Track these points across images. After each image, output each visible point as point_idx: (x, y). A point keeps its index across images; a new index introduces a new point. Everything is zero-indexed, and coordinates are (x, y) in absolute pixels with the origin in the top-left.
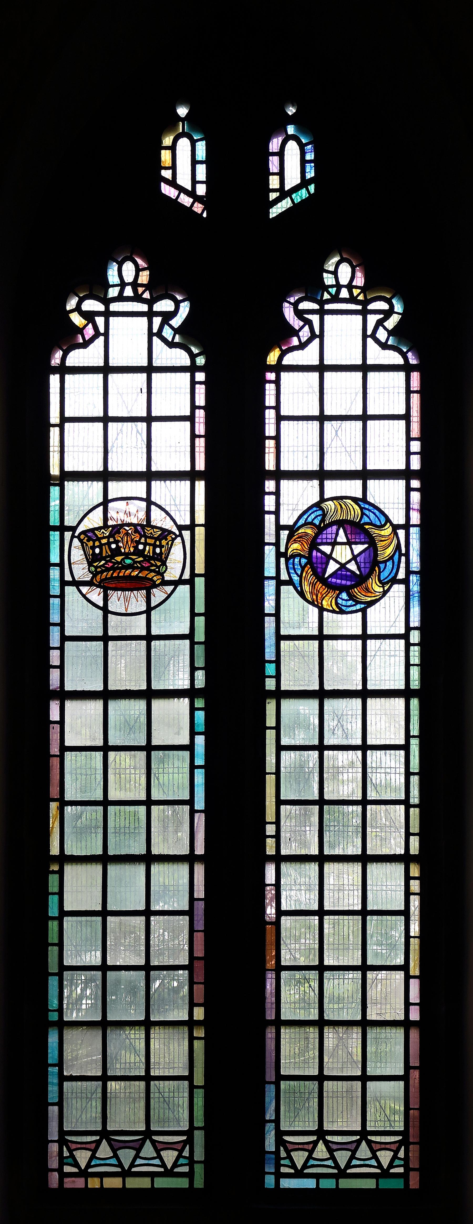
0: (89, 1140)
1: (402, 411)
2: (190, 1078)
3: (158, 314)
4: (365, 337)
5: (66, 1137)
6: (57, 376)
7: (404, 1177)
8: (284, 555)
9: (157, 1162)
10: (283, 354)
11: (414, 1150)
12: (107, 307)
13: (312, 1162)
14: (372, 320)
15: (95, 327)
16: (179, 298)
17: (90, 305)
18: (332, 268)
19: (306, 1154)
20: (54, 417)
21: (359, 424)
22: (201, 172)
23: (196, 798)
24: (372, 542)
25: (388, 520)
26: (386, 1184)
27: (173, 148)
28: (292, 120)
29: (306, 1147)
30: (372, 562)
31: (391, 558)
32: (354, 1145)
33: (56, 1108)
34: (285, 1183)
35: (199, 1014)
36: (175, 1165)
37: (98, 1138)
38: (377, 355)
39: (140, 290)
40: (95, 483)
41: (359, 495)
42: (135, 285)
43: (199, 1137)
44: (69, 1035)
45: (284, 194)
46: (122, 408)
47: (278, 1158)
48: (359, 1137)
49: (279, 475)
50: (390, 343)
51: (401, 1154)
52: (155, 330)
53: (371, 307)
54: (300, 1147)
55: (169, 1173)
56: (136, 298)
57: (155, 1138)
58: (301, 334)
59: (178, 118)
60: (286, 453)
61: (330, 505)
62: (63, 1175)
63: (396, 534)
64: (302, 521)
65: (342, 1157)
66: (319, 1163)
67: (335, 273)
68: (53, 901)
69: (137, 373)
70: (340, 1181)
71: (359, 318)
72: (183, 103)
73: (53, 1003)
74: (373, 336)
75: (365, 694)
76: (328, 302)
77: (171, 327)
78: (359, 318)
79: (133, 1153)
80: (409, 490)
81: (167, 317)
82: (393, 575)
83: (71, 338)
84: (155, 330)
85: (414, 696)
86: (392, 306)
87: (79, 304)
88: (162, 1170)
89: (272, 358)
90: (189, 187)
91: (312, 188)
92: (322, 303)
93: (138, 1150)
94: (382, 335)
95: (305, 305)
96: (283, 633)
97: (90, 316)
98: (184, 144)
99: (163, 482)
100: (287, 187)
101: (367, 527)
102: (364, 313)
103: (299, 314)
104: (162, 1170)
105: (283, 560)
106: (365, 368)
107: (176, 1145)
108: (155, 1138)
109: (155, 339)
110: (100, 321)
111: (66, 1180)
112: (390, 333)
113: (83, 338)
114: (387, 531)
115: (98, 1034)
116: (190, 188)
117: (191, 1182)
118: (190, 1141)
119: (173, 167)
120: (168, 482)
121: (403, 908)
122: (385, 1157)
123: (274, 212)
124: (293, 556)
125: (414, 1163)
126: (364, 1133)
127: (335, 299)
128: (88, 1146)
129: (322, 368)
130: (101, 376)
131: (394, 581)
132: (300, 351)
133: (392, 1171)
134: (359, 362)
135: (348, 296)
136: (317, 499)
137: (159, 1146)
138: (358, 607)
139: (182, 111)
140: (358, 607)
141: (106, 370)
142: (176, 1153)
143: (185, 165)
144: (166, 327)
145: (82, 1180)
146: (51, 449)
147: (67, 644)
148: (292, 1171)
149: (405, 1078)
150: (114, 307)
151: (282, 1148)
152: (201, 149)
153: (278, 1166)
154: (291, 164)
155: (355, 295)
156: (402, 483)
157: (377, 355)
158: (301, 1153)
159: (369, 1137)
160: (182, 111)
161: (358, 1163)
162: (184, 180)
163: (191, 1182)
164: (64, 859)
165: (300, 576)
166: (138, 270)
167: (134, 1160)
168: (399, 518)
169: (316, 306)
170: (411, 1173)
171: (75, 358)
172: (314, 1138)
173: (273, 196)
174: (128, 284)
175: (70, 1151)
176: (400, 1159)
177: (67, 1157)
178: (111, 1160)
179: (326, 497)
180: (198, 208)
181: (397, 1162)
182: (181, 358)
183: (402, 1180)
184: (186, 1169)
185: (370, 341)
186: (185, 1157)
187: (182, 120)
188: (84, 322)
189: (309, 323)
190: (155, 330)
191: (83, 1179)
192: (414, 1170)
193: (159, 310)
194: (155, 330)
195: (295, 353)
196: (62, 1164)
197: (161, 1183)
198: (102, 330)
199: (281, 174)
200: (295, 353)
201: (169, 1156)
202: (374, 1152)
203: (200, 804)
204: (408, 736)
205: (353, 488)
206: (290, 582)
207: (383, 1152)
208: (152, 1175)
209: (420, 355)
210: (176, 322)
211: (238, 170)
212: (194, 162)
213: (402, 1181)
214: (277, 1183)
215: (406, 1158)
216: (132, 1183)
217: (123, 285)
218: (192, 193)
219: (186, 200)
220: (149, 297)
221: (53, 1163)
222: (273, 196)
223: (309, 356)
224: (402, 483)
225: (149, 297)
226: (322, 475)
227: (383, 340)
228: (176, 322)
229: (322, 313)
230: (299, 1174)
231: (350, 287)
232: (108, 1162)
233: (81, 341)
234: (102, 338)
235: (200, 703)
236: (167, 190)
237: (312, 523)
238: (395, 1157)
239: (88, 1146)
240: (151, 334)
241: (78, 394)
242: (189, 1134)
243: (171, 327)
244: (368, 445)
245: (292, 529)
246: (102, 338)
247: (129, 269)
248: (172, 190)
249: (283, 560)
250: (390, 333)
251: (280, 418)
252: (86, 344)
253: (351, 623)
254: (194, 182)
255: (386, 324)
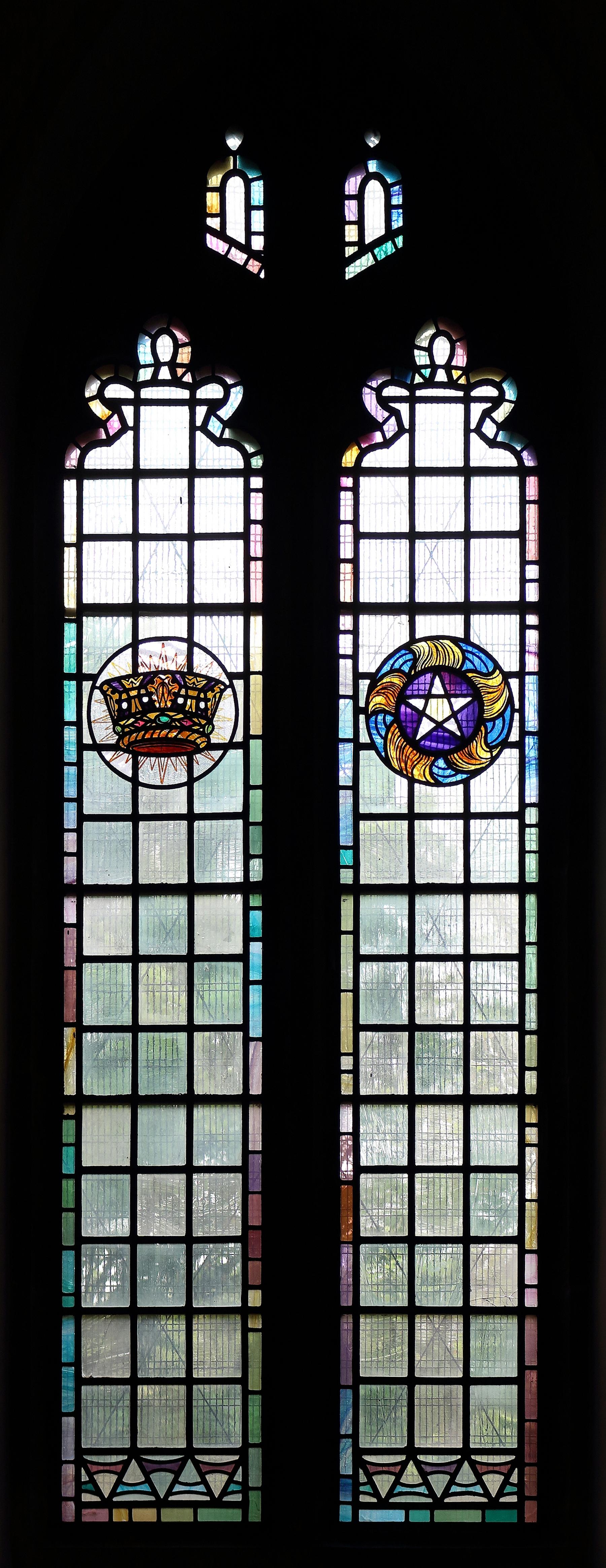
0: (113, 1461)
1: (516, 527)
2: (243, 1381)
3: (203, 402)
4: (467, 431)
5: (85, 1457)
6: (73, 482)
7: (518, 1507)
8: (364, 710)
9: (201, 1488)
10: (363, 453)
11: (531, 1473)
12: (137, 394)
13: (399, 1489)
14: (477, 409)
15: (122, 419)
16: (230, 381)
17: (115, 391)
18: (425, 344)
19: (393, 1478)
20: (70, 534)
21: (460, 543)
22: (258, 220)
23: (251, 1023)
24: (476, 695)
25: (497, 666)
26: (494, 1517)
27: (221, 190)
28: (374, 154)
29: (392, 1469)
30: (476, 721)
31: (501, 715)
32: (454, 1467)
33: (72, 1420)
34: (366, 1516)
35: (255, 1298)
36: (225, 1492)
37: (126, 1457)
38: (483, 455)
39: (180, 371)
40: (122, 618)
41: (460, 634)
42: (173, 365)
43: (255, 1456)
44: (89, 1325)
45: (364, 249)
46: (156, 523)
47: (356, 1484)
48: (459, 1457)
49: (358, 608)
50: (499, 439)
51: (514, 1479)
52: (199, 423)
53: (475, 393)
54: (384, 1469)
55: (216, 1503)
56: (175, 381)
57: (198, 1457)
58: (385, 427)
59: (229, 152)
60: (367, 581)
61: (423, 647)
62: (81, 1506)
63: (508, 685)
64: (387, 668)
65: (439, 1482)
66: (409, 1490)
67: (429, 350)
68: (68, 1154)
69: (176, 478)
70: (436, 1512)
71: (461, 407)
72: (234, 132)
73: (68, 1285)
74: (478, 430)
75: (467, 889)
76: (420, 386)
77: (219, 419)
78: (461, 407)
79: (170, 1477)
80: (524, 627)
81: (214, 406)
82: (503, 736)
83: (90, 433)
84: (199, 422)
85: (530, 892)
86: (502, 392)
87: (101, 390)
88: (208, 1498)
89: (349, 458)
90: (242, 240)
91: (399, 241)
92: (412, 388)
93: (177, 1473)
94: (489, 429)
95: (391, 391)
96: (362, 810)
97: (115, 405)
98: (235, 185)
99: (208, 617)
100: (368, 240)
101: (470, 675)
102: (467, 401)
103: (384, 402)
104: (208, 1498)
105: (362, 718)
106: (467, 472)
107: (226, 1467)
108: (198, 1457)
109: (198, 434)
110: (128, 411)
111: (85, 1512)
112: (500, 426)
113: (107, 433)
114: (496, 680)
115: (125, 1325)
116: (243, 241)
117: (245, 1515)
118: (243, 1462)
119: (222, 214)
120: (215, 618)
121: (516, 1163)
122: (493, 1482)
123: (352, 271)
124: (376, 713)
125: (531, 1490)
126: (466, 1452)
127: (430, 383)
128: (112, 1468)
129: (412, 472)
130: (129, 482)
131: (505, 744)
132: (385, 450)
133: (502, 1500)
134: (460, 464)
135: (446, 380)
136: (406, 639)
137: (204, 1469)
138: (459, 777)
139: (234, 143)
140: (459, 777)
141: (136, 474)
142: (225, 1477)
143: (236, 211)
144: (213, 419)
145: (106, 1511)
146: (66, 575)
147: (86, 825)
148: (374, 1500)
149: (519, 1381)
150: (147, 393)
151: (361, 1471)
152: (258, 191)
153: (356, 1493)
154: (373, 210)
155: (455, 378)
156: (515, 619)
157: (483, 455)
158: (385, 1477)
159: (473, 1457)
160: (234, 143)
161: (459, 1489)
162: (236, 231)
163: (245, 1515)
164: (82, 1100)
165: (385, 738)
166: (177, 346)
167: (172, 1486)
168: (511, 664)
169: (405, 393)
170: (527, 1503)
171: (97, 459)
172: (403, 1458)
173: (350, 251)
174: (165, 364)
175: (90, 1474)
176: (512, 1484)
177: (86, 1483)
178: (143, 1486)
179: (417, 637)
180: (254, 266)
181: (508, 1489)
182: (232, 458)
183: (515, 1512)
184: (238, 1498)
185: (474, 437)
186: (237, 1483)
187: (234, 153)
188: (108, 412)
189: (396, 414)
190: (199, 423)
191: (106, 1511)
192: (530, 1498)
193: (203, 397)
194: (199, 422)
195: (379, 452)
196: (79, 1491)
197: (206, 1515)
198: (131, 423)
199: (360, 222)
200: (379, 452)
201: (217, 1482)
202: (479, 1476)
203: (256, 1030)
204: (522, 943)
205: (453, 625)
206: (371, 746)
207: (491, 1476)
208: (195, 1506)
209: (538, 455)
210: (226, 412)
211: (305, 217)
212: (249, 208)
213: (514, 1513)
214: (355, 1515)
215: (521, 1484)
216: (170, 1515)
217: (157, 365)
218: (245, 248)
219: (238, 257)
220: (191, 381)
221: (68, 1490)
222: (350, 251)
223: (396, 456)
224: (515, 619)
225: (191, 381)
226: (412, 609)
227: (491, 436)
228: (226, 412)
229: (412, 401)
230: (383, 1504)
231: (448, 367)
232: (138, 1488)
233: (104, 437)
234: (130, 434)
235: (256, 901)
236: (214, 244)
237: (399, 670)
238: (506, 1483)
239: (112, 1468)
240: (193, 428)
241: (101, 505)
242: (242, 1452)
243: (219, 419)
244: (472, 570)
245: (374, 678)
246: (130, 434)
247: (165, 345)
248: (221, 243)
249: (362, 718)
250: (500, 426)
251: (358, 536)
252: (110, 441)
253: (449, 799)
254: (249, 233)
255: (494, 415)
